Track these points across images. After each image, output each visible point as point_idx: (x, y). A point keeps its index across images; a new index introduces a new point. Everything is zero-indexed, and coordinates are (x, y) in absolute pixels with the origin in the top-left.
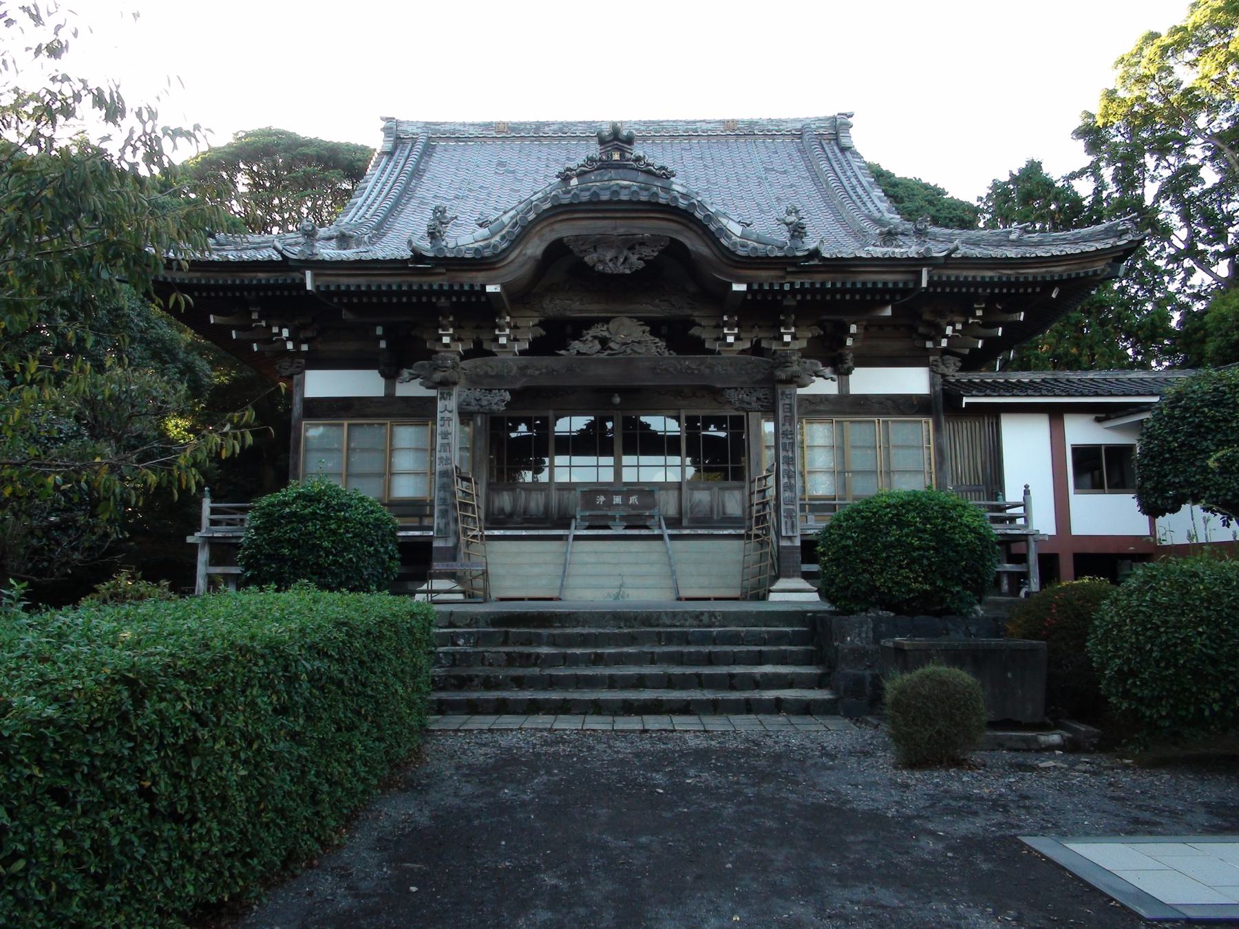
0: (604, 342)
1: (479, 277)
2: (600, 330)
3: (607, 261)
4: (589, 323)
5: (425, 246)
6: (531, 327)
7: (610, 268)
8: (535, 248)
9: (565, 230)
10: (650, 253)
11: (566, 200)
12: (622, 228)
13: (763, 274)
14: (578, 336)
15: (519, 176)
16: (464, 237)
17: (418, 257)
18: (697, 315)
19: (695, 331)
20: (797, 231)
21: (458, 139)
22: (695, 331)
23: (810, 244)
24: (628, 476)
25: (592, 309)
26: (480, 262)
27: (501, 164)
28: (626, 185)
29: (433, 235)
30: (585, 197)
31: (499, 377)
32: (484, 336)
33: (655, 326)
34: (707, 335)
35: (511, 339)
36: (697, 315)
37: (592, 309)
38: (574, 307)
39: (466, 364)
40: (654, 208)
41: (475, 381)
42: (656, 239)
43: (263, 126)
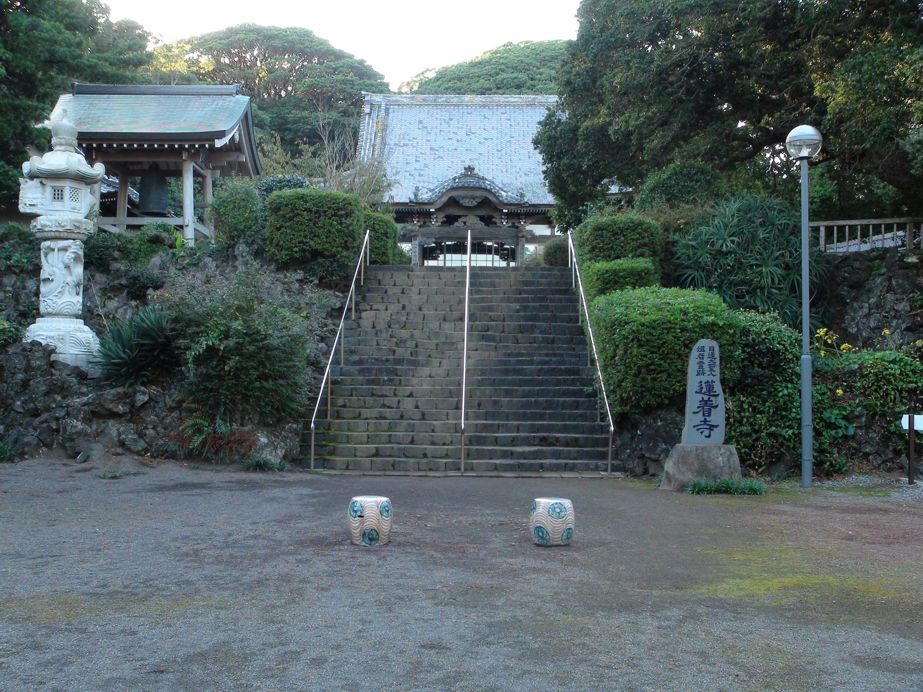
0: (465, 223)
1: (428, 207)
2: (463, 219)
3: (466, 203)
4: (460, 217)
5: (412, 197)
6: (441, 217)
7: (467, 205)
8: (445, 199)
9: (454, 194)
10: (479, 200)
11: (455, 185)
12: (471, 193)
13: (513, 207)
14: (457, 221)
15: (429, 130)
16: (425, 196)
17: (411, 202)
18: (494, 214)
19: (494, 220)
20: (522, 195)
21: (399, 105)
22: (494, 220)
23: (526, 200)
24: (448, 264)
25: (461, 213)
26: (429, 204)
27: (420, 122)
28: (473, 182)
29: (416, 195)
30: (460, 185)
31: (431, 234)
32: (427, 221)
33: (482, 218)
34: (498, 221)
35: (435, 223)
36: (494, 214)
37: (461, 213)
38: (455, 212)
39: (422, 229)
40: (480, 188)
41: (424, 235)
42: (481, 196)
43: (234, 22)
